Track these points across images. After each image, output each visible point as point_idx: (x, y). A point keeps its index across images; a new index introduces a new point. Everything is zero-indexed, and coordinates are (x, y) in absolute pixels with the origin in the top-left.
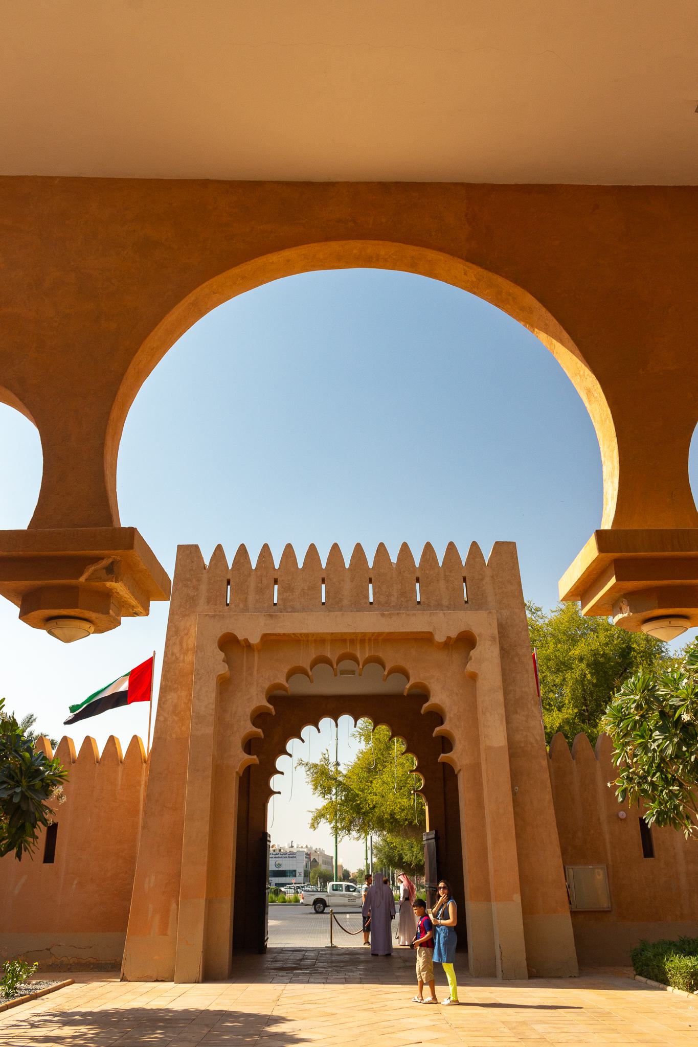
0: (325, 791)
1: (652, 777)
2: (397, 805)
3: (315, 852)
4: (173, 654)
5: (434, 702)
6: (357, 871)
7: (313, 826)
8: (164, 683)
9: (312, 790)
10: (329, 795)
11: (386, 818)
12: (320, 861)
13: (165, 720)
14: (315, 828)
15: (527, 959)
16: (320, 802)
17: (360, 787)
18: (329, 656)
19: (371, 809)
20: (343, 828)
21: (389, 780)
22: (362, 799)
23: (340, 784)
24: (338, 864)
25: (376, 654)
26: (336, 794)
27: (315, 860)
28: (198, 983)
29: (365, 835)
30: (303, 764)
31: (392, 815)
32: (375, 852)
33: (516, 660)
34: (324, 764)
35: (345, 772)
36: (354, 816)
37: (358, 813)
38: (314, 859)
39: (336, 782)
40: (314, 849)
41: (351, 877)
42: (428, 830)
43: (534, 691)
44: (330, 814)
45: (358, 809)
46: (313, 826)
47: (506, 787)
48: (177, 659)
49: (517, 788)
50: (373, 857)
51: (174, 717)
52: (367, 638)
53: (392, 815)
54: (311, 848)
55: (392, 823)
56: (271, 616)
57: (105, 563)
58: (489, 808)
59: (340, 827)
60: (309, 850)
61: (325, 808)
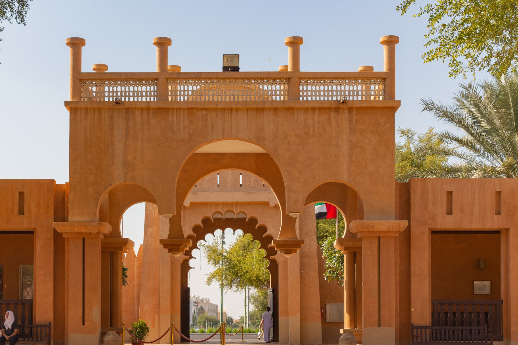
0: (216, 262)
1: (337, 272)
2: (261, 271)
3: (202, 301)
4: (149, 210)
5: (268, 233)
6: (240, 318)
7: (208, 283)
8: (146, 224)
9: (207, 262)
10: (218, 265)
11: (254, 279)
12: (206, 308)
13: (148, 240)
14: (209, 285)
15: (301, 338)
16: (212, 269)
17: (238, 260)
18: (221, 211)
19: (244, 273)
20: (227, 285)
21: (256, 255)
22: (239, 268)
23: (225, 257)
24: (223, 312)
25: (243, 211)
26: (222, 264)
27: (202, 308)
28: (169, 344)
29: (241, 289)
30: (202, 245)
31: (258, 277)
32: (252, 300)
33: (308, 214)
34: (215, 246)
35: (228, 250)
36: (234, 277)
37: (237, 276)
38: (201, 307)
39: (222, 257)
40: (201, 298)
41: (234, 323)
42: (271, 287)
43: (315, 228)
44: (219, 276)
45: (236, 274)
46: (208, 283)
47: (298, 271)
48: (151, 212)
49: (303, 271)
50: (250, 304)
51: (152, 239)
52: (239, 203)
53: (258, 277)
54: (198, 297)
55: (257, 282)
56: (194, 193)
57: (185, 244)
58: (290, 279)
59: (225, 284)
60: (196, 299)
61: (216, 272)
